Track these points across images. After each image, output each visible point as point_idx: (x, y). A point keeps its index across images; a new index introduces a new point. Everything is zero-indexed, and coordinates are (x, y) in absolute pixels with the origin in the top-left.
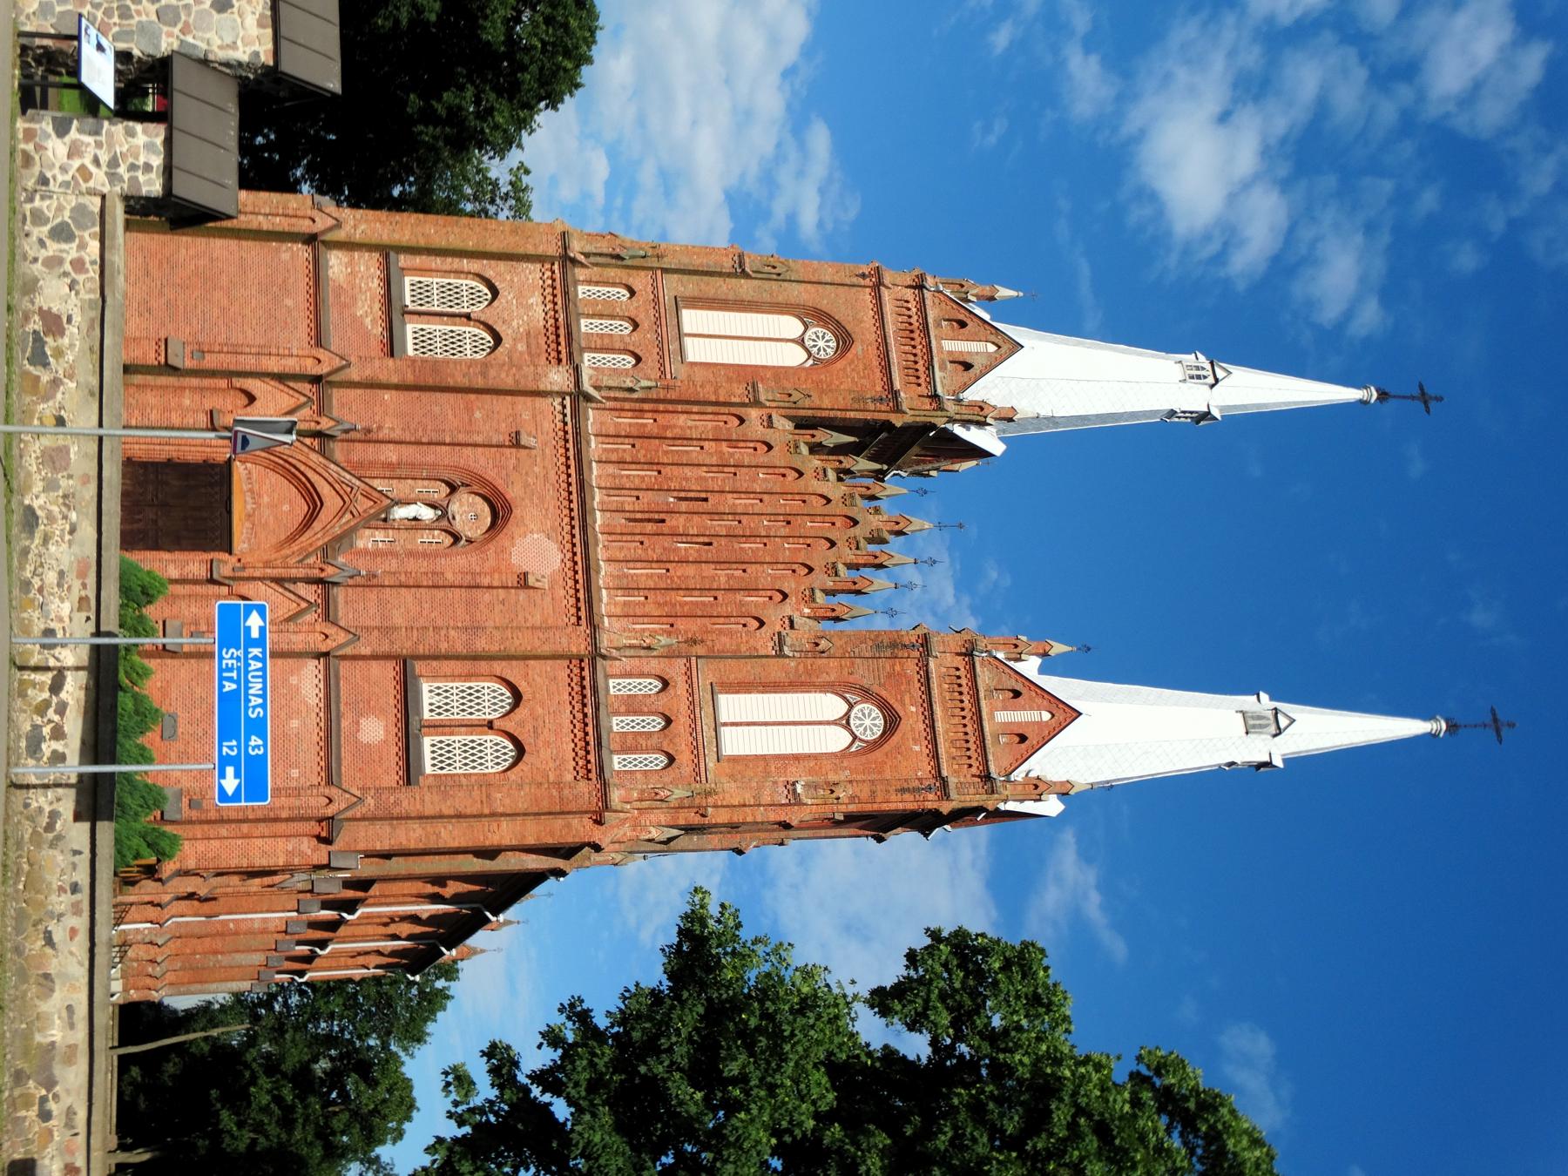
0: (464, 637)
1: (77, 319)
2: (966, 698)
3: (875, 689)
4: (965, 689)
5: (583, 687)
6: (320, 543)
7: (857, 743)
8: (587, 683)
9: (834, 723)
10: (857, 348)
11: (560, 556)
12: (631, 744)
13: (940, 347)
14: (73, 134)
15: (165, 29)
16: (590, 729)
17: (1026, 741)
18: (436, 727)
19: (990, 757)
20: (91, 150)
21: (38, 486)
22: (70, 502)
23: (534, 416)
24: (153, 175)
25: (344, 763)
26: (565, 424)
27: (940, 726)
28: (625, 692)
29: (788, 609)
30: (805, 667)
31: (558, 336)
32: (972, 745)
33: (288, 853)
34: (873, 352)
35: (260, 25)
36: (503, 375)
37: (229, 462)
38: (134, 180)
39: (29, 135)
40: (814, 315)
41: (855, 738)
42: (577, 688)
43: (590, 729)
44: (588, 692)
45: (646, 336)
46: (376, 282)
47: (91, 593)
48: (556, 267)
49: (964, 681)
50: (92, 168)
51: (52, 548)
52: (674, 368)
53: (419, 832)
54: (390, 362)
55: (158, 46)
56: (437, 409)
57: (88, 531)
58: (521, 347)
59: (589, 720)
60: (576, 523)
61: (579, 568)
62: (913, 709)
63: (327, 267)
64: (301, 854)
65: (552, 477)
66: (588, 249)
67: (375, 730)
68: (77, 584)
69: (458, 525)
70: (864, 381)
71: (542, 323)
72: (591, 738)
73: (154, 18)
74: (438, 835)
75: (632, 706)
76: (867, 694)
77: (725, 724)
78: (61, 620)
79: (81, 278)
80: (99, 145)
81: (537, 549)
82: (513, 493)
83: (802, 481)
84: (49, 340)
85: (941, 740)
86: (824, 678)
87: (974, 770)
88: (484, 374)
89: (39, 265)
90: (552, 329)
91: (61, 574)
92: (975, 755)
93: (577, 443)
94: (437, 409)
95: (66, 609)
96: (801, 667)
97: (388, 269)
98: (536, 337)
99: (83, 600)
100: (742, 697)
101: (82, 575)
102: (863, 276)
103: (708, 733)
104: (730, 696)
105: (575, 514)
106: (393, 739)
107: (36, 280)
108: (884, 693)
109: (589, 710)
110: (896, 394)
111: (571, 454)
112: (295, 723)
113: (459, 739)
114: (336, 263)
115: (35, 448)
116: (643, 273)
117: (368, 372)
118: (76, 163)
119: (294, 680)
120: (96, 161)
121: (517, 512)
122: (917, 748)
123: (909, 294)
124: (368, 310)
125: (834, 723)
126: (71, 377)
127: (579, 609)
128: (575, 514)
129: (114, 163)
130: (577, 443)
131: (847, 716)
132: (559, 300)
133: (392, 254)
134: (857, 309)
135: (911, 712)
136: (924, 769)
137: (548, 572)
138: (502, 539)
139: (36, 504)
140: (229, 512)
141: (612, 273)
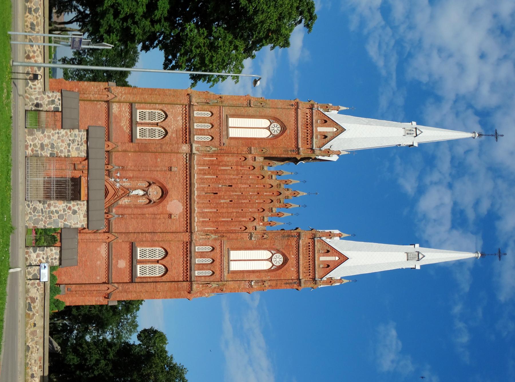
0: (151, 236)
1: (39, 298)
2: (311, 253)
3: (281, 250)
4: (311, 250)
5: (187, 251)
6: (107, 206)
7: (274, 267)
8: (188, 249)
9: (267, 260)
10: (288, 132)
11: (182, 208)
12: (202, 267)
13: (317, 130)
14: (38, 252)
15: (60, 220)
16: (188, 264)
17: (329, 267)
18: (141, 262)
19: (316, 272)
20: (42, 255)
21: (30, 340)
22: (37, 343)
23: (177, 160)
24: (57, 260)
25: (113, 274)
26: (187, 163)
27: (301, 262)
28: (200, 251)
29: (255, 224)
30: (259, 243)
31: (186, 132)
32: (311, 268)
33: (96, 301)
34: (293, 133)
35: (84, 217)
36: (167, 148)
37: (80, 177)
38: (52, 262)
39: (27, 253)
40: (274, 119)
41: (273, 265)
42: (185, 251)
43: (188, 264)
44: (188, 252)
45: (216, 129)
46: (128, 113)
47: (42, 365)
48: (187, 107)
49: (311, 247)
50: (42, 260)
51: (33, 355)
52: (224, 140)
53: (135, 295)
54: (131, 144)
55: (58, 226)
56: (146, 158)
57: (41, 350)
58: (174, 135)
59: (188, 261)
60: (188, 197)
61: (188, 212)
62: (293, 256)
63: (112, 109)
64: (100, 301)
65: (182, 181)
66: (198, 101)
67: (123, 264)
68: (39, 362)
69: (151, 197)
70: (289, 143)
71: (181, 126)
72: (188, 267)
73: (57, 218)
74: (141, 296)
75: (202, 255)
76: (278, 251)
77: (232, 260)
78: (35, 371)
79: (39, 288)
80: (44, 254)
81: (175, 206)
82: (169, 186)
83: (264, 180)
84: (32, 304)
85: (301, 267)
86: (265, 246)
87: (311, 277)
88: (161, 148)
89: (29, 285)
90: (184, 129)
91: (35, 360)
92: (311, 272)
93: (190, 170)
94: (146, 158)
95: (36, 368)
96: (258, 243)
97: (132, 108)
98: (179, 132)
99: (40, 366)
100: (238, 251)
101: (40, 360)
102: (292, 105)
103: (225, 264)
104: (234, 251)
105: (188, 194)
106: (128, 267)
107: (29, 289)
108: (284, 251)
109: (188, 258)
110: (299, 149)
111: (188, 173)
112: (99, 262)
113: (148, 265)
114: (115, 108)
115: (29, 331)
116: (216, 107)
117: (124, 148)
118: (38, 259)
119: (99, 249)
120: (43, 258)
121: (169, 193)
122: (293, 269)
123: (308, 111)
124: (125, 124)
125: (267, 260)
126: (37, 313)
127: (187, 226)
128: (188, 194)
129: (47, 258)
130: (190, 170)
131: (271, 258)
132: (187, 119)
133: (133, 104)
134: (289, 119)
135: (292, 257)
136: (294, 276)
137: (179, 213)
138: (164, 202)
139: (29, 345)
140: (80, 195)
141: (206, 107)
